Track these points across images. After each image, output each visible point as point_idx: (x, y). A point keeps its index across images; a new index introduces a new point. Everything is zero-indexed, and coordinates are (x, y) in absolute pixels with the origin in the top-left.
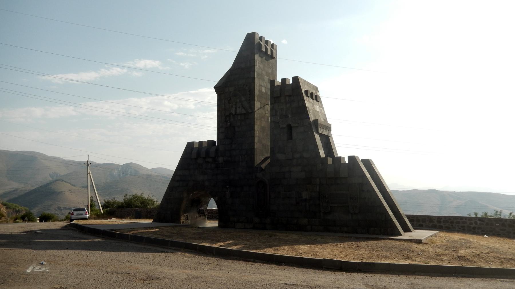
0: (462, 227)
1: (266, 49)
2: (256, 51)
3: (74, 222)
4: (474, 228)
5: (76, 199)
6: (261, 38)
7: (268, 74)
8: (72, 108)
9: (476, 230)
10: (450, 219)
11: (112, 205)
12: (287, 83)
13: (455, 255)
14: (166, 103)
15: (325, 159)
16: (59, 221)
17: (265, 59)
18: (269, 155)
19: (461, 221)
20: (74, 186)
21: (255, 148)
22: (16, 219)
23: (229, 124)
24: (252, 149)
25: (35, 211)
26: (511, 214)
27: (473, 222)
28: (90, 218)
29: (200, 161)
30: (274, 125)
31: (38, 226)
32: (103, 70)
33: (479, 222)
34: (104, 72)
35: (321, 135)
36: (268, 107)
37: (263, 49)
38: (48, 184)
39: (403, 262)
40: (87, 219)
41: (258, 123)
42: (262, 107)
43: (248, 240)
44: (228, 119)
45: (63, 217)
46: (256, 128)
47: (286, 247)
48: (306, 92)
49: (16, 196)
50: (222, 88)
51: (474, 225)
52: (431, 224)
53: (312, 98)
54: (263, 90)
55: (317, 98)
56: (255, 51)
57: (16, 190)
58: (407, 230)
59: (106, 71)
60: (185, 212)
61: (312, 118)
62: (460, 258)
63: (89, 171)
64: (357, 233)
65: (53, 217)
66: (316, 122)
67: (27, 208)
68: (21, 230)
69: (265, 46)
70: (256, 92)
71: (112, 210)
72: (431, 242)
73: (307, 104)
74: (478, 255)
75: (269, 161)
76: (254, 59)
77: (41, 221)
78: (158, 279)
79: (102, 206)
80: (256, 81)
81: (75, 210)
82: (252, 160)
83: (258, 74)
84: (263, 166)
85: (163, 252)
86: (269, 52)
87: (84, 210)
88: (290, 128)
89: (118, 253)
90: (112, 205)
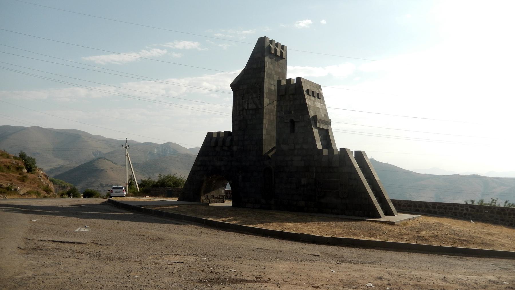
2: (266, 53)
3: (112, 198)
4: (465, 214)
5: (118, 177)
6: (271, 42)
7: (277, 73)
8: (114, 88)
9: (467, 216)
10: (444, 206)
11: (148, 184)
12: (292, 83)
13: (416, 235)
14: (205, 84)
15: (321, 150)
16: (101, 197)
17: (275, 60)
18: (275, 146)
19: (454, 207)
20: (116, 164)
22: (62, 195)
24: (261, 140)
25: (79, 187)
26: (506, 202)
27: (464, 208)
28: (127, 196)
29: (218, 149)
30: (280, 119)
31: (82, 201)
32: (144, 51)
33: (470, 209)
34: (145, 53)
35: (320, 130)
36: (275, 103)
37: (273, 52)
39: (367, 239)
40: (124, 196)
41: (267, 117)
45: (105, 194)
46: (265, 121)
47: (274, 224)
48: (308, 91)
49: (62, 172)
51: (465, 211)
52: (426, 209)
53: (313, 96)
54: (273, 88)
56: (266, 54)
57: (62, 167)
58: (388, 212)
59: (147, 52)
60: (205, 192)
61: (312, 114)
62: (422, 238)
63: (127, 153)
64: (345, 215)
65: (95, 194)
66: (315, 117)
67: (71, 185)
68: (69, 204)
69: (275, 48)
70: (266, 90)
71: (148, 188)
72: (405, 223)
73: (308, 102)
76: (264, 61)
77: (84, 197)
79: (138, 185)
80: (266, 80)
81: (114, 188)
82: (261, 149)
83: (268, 74)
84: (270, 155)
85: (177, 224)
86: (279, 54)
88: (292, 122)
89: (141, 223)
90: (148, 184)
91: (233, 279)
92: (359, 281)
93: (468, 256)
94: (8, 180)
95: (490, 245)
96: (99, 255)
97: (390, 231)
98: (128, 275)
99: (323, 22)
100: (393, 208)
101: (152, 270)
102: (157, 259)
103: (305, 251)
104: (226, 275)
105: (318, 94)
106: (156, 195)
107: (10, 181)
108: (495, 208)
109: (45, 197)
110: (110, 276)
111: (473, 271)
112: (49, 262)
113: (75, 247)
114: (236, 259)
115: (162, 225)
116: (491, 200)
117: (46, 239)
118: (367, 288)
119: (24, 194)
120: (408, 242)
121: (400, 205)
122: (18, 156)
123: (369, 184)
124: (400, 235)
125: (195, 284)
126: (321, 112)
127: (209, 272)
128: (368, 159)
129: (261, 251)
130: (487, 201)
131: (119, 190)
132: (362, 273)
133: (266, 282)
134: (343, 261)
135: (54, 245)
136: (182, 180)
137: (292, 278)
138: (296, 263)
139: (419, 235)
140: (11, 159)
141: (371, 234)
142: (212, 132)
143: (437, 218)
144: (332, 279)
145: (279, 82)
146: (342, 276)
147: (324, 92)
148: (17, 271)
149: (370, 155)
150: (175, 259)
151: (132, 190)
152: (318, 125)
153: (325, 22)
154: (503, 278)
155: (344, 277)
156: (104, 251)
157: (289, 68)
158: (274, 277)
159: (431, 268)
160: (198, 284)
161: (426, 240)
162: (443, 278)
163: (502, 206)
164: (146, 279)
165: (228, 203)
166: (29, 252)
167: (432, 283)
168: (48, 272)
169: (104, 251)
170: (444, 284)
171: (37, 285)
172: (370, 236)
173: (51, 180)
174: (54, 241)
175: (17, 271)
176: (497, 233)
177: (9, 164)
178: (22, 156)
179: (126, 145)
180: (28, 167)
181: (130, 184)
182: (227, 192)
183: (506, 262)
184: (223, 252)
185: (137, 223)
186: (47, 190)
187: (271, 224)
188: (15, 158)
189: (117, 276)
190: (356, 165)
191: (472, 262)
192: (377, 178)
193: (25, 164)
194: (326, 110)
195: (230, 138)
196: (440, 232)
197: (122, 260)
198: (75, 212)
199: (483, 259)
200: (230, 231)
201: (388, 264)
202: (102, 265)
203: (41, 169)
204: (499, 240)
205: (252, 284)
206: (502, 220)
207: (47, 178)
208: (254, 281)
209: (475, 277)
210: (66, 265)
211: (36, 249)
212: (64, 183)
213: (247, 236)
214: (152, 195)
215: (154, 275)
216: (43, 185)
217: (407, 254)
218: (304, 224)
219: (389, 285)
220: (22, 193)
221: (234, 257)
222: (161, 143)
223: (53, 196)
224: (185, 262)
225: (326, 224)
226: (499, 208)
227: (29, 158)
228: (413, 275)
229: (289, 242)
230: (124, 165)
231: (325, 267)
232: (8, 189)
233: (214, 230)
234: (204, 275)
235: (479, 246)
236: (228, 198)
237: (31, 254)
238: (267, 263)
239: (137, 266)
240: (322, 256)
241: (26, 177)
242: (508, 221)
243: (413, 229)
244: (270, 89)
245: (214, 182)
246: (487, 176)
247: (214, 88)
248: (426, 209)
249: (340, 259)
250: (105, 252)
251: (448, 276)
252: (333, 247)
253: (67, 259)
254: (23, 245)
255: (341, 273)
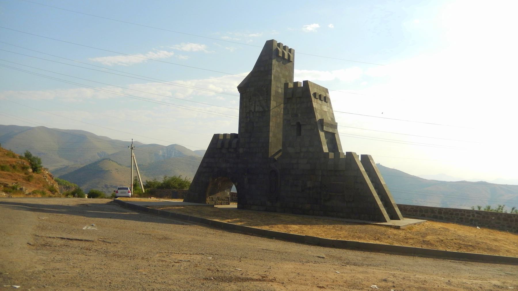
0: (460, 218)
1: (283, 54)
4: (472, 220)
5: (123, 179)
6: (279, 45)
11: (153, 186)
12: (299, 86)
13: (421, 239)
14: (211, 86)
15: (328, 154)
16: (105, 198)
17: (283, 63)
18: (281, 148)
20: (121, 165)
21: (270, 141)
23: (248, 119)
25: (84, 188)
26: (513, 209)
27: (471, 214)
28: (132, 196)
31: (87, 200)
32: (150, 52)
33: (476, 215)
35: (326, 133)
36: (282, 106)
37: (281, 55)
38: (96, 163)
39: (372, 242)
42: (278, 106)
43: (252, 219)
44: (248, 115)
45: (110, 195)
46: (271, 124)
47: (280, 226)
48: (315, 94)
50: (244, 88)
51: (471, 217)
52: (433, 214)
53: (320, 99)
55: (326, 99)
56: (274, 56)
57: (67, 167)
58: (394, 216)
60: (211, 194)
61: (318, 117)
62: (428, 243)
63: (133, 154)
66: (322, 121)
67: (76, 185)
68: (75, 204)
69: (283, 51)
70: (273, 93)
71: (153, 189)
72: (410, 228)
74: (442, 240)
75: (280, 154)
76: (271, 64)
78: (171, 239)
79: (144, 186)
80: (273, 83)
81: (119, 189)
82: (267, 152)
83: (275, 77)
84: (276, 157)
86: (286, 57)
87: (127, 189)
88: (299, 126)
89: (147, 223)
90: (153, 186)
91: (239, 278)
92: (363, 283)
93: (474, 262)
94: (13, 180)
95: (495, 251)
96: (106, 252)
97: (395, 235)
98: (136, 271)
99: (331, 26)
100: (399, 213)
101: (159, 268)
102: (164, 257)
103: (310, 253)
104: (232, 274)
105: (325, 98)
106: (161, 197)
107: (16, 180)
108: (501, 214)
109: (50, 197)
110: (119, 272)
111: (478, 276)
112: (59, 257)
113: (83, 244)
114: (242, 259)
115: (168, 225)
116: (498, 207)
117: (55, 237)
118: (371, 289)
119: (30, 194)
120: (414, 247)
121: (405, 210)
122: (24, 156)
123: (375, 188)
124: (405, 239)
125: (202, 281)
126: (328, 115)
127: (215, 271)
128: (374, 163)
129: (266, 252)
130: (494, 207)
131: (125, 191)
132: (367, 275)
133: (271, 281)
134: (347, 263)
135: (62, 242)
136: (187, 182)
137: (297, 277)
138: (301, 264)
139: (425, 239)
140: (17, 158)
141: (377, 237)
142: (219, 134)
143: (443, 224)
144: (337, 280)
145: (286, 85)
146: (347, 277)
147: (332, 95)
148: (28, 265)
149: (377, 160)
150: (182, 258)
151: (137, 191)
152: (325, 128)
153: (333, 27)
154: (507, 283)
155: (349, 279)
156: (112, 249)
157: (296, 71)
158: (280, 277)
159: (436, 272)
160: (205, 281)
161: (431, 244)
162: (447, 281)
163: (509, 212)
164: (153, 276)
165: (234, 205)
166: (38, 248)
167: (436, 286)
168: (58, 267)
169: (112, 249)
170: (448, 287)
171: (48, 279)
172: (376, 240)
173: (56, 181)
174: (62, 238)
175: (28, 265)
176: (503, 239)
177: (14, 164)
178: (28, 156)
179: (132, 146)
180: (34, 167)
181: (135, 185)
182: (232, 194)
183: (512, 268)
184: (229, 252)
185: (143, 222)
186: (52, 191)
187: (276, 226)
188: (21, 157)
189: (125, 272)
190: (362, 169)
191: (478, 267)
192: (383, 182)
193: (30, 164)
194: (333, 114)
195: (236, 140)
196: (445, 237)
197: (129, 258)
198: (81, 210)
199: (489, 264)
200: (236, 233)
201: (393, 267)
202: (110, 262)
203: (47, 169)
204: (505, 246)
205: (258, 282)
206: (509, 227)
207: (53, 178)
208: (260, 280)
209: (479, 282)
210: (75, 261)
211: (44, 245)
212: (69, 184)
213: (252, 237)
214: (157, 197)
215: (161, 273)
216: (48, 185)
217: (412, 258)
218: (309, 226)
219: (394, 287)
220: (27, 192)
221: (239, 257)
222: (166, 144)
223: (58, 196)
224: (192, 261)
225: (331, 227)
226: (506, 214)
227: (34, 158)
228: (418, 278)
229: (294, 244)
230: (129, 167)
231: (332, 268)
232: (13, 188)
233: (220, 231)
234: (210, 273)
235: (485, 251)
236: (233, 201)
237: (40, 249)
238: (272, 263)
239: (145, 263)
240: (327, 257)
241: (31, 176)
242: (514, 228)
243: (418, 233)
244: (277, 92)
245: (220, 184)
246: (495, 183)
247: (221, 90)
248: (433, 214)
249: (345, 262)
250: (112, 249)
251: (452, 280)
252: (338, 250)
253: (76, 256)
254: (32, 242)
255: (346, 275)
